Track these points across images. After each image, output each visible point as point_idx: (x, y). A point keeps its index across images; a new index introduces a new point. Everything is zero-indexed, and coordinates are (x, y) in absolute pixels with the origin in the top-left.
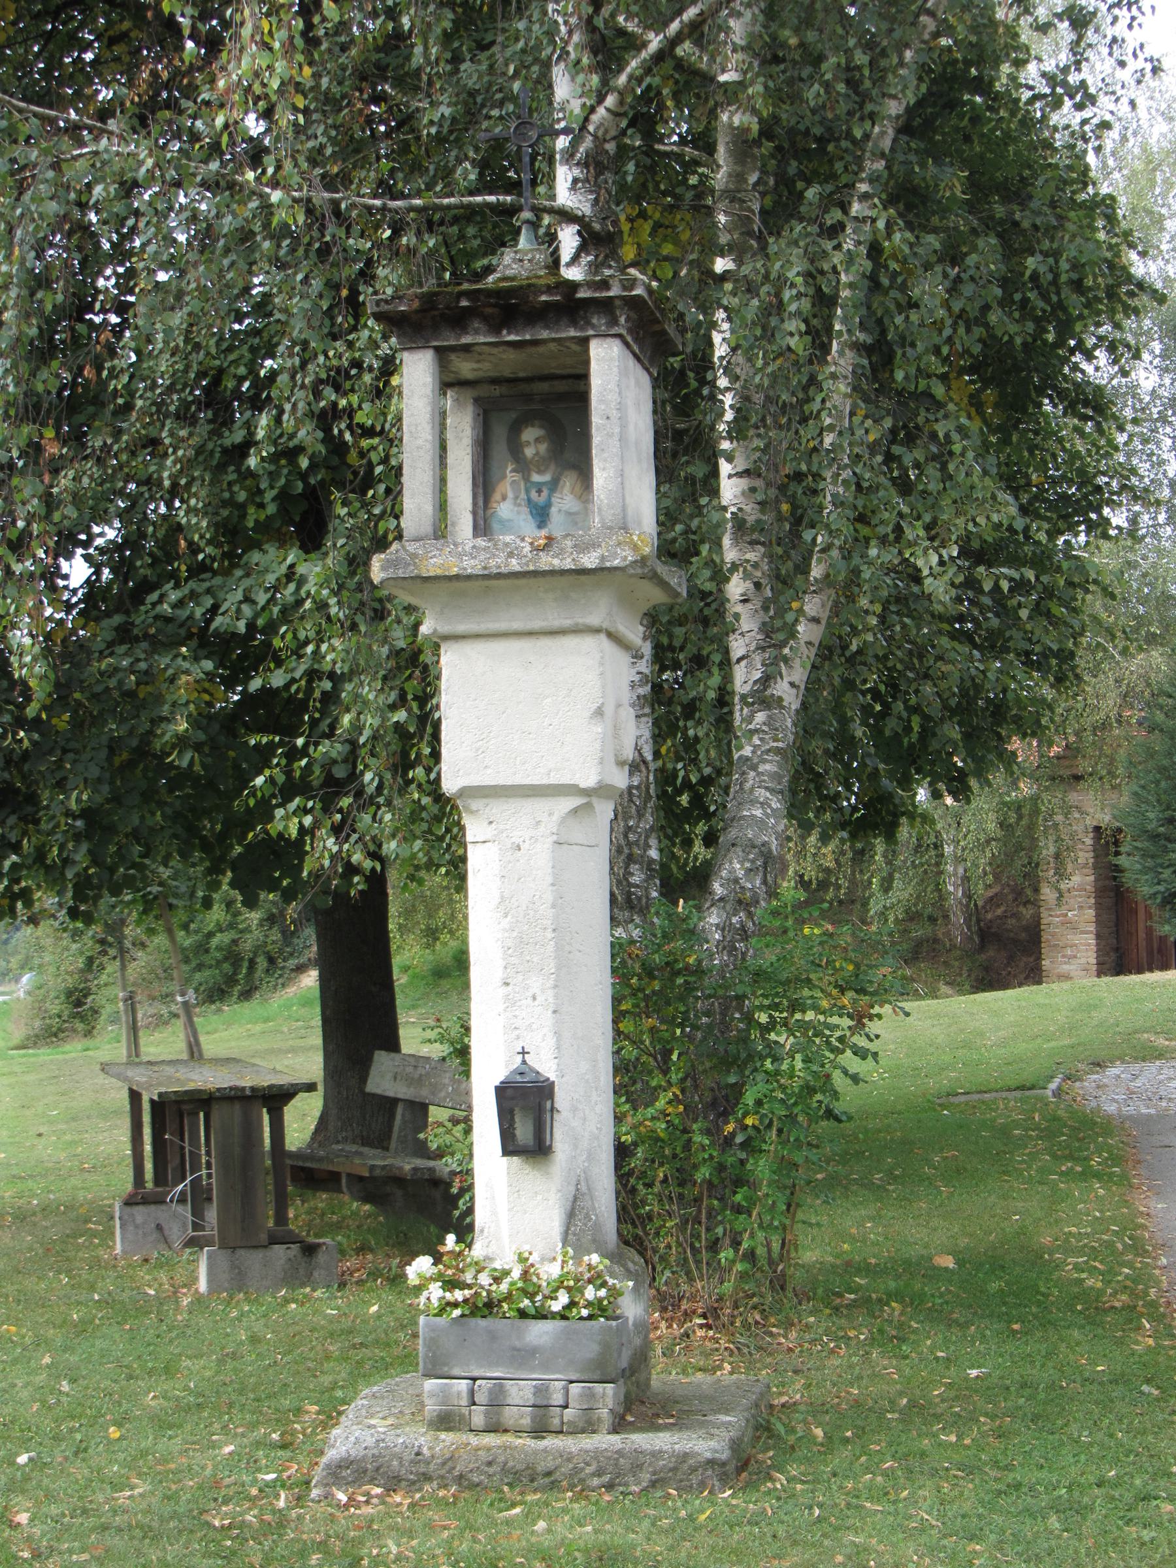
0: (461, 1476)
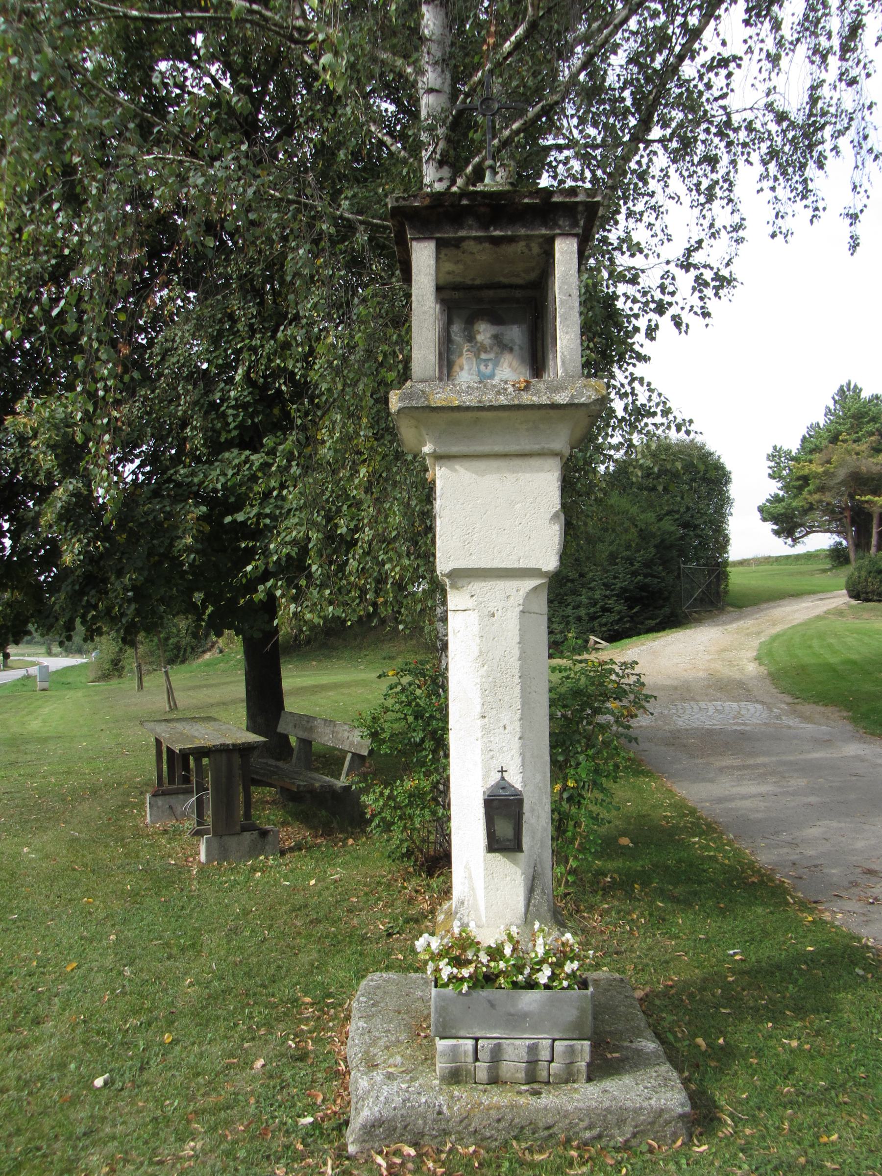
0: (476, 1131)
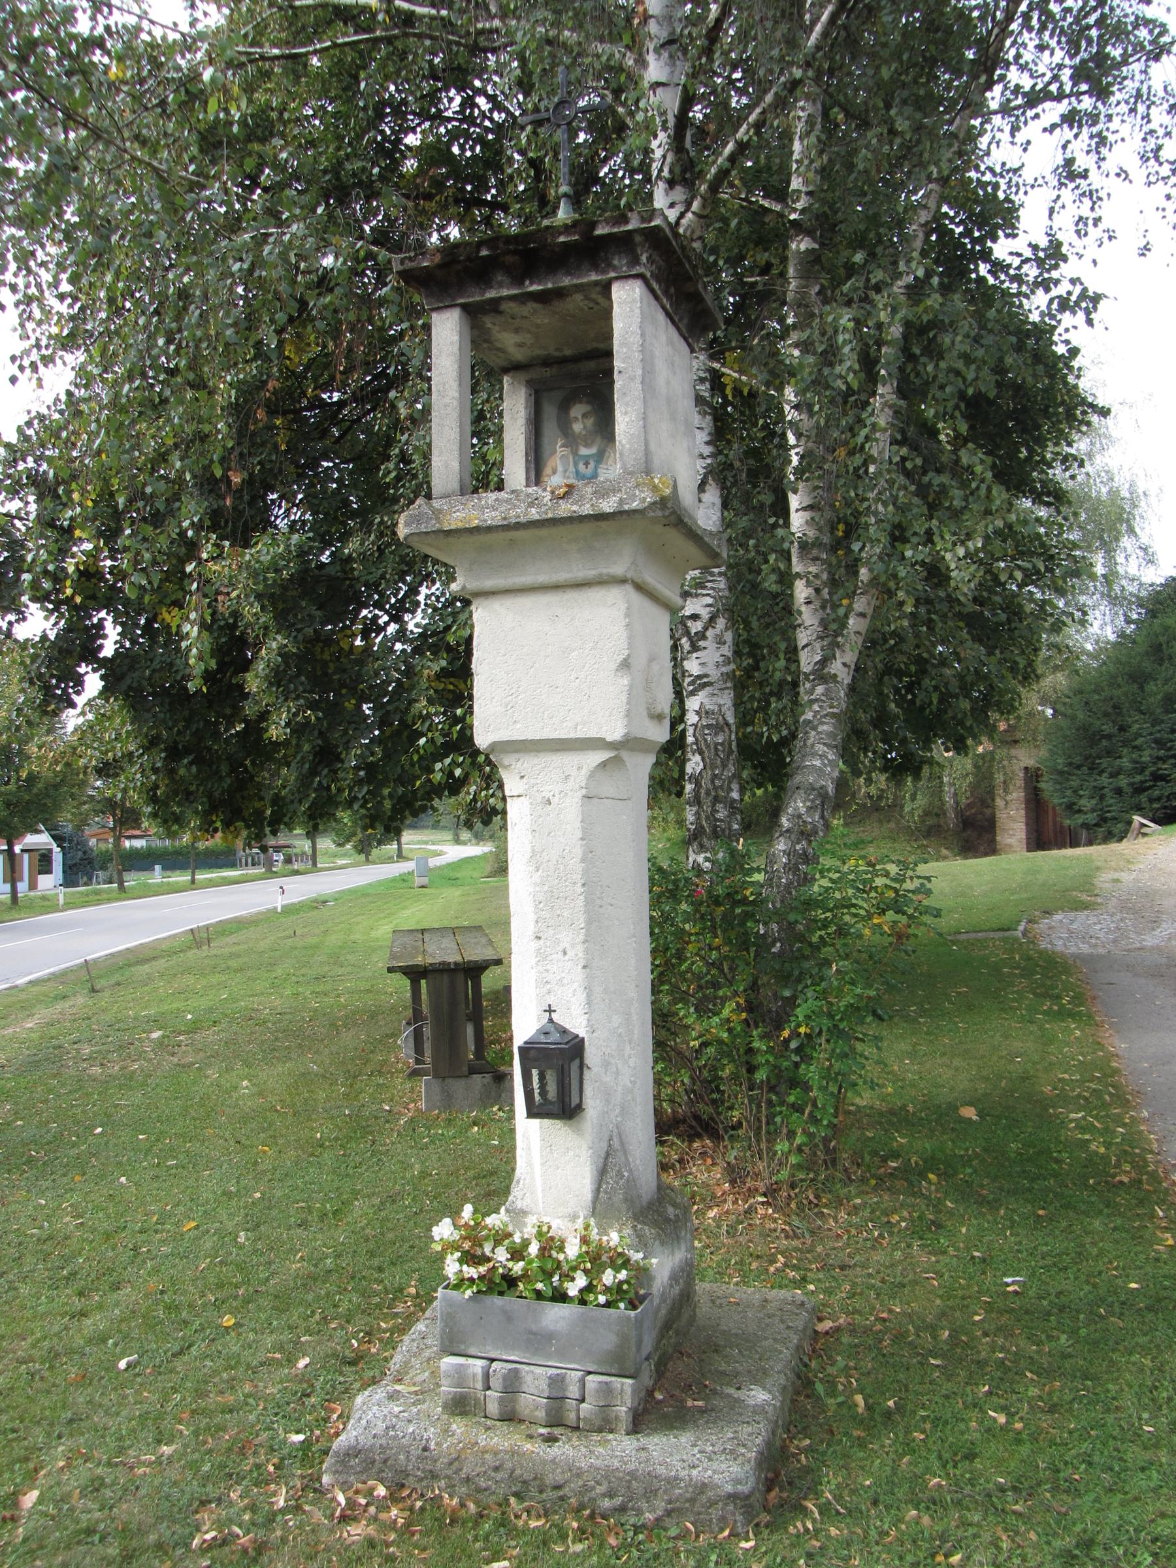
0: (468, 1479)
